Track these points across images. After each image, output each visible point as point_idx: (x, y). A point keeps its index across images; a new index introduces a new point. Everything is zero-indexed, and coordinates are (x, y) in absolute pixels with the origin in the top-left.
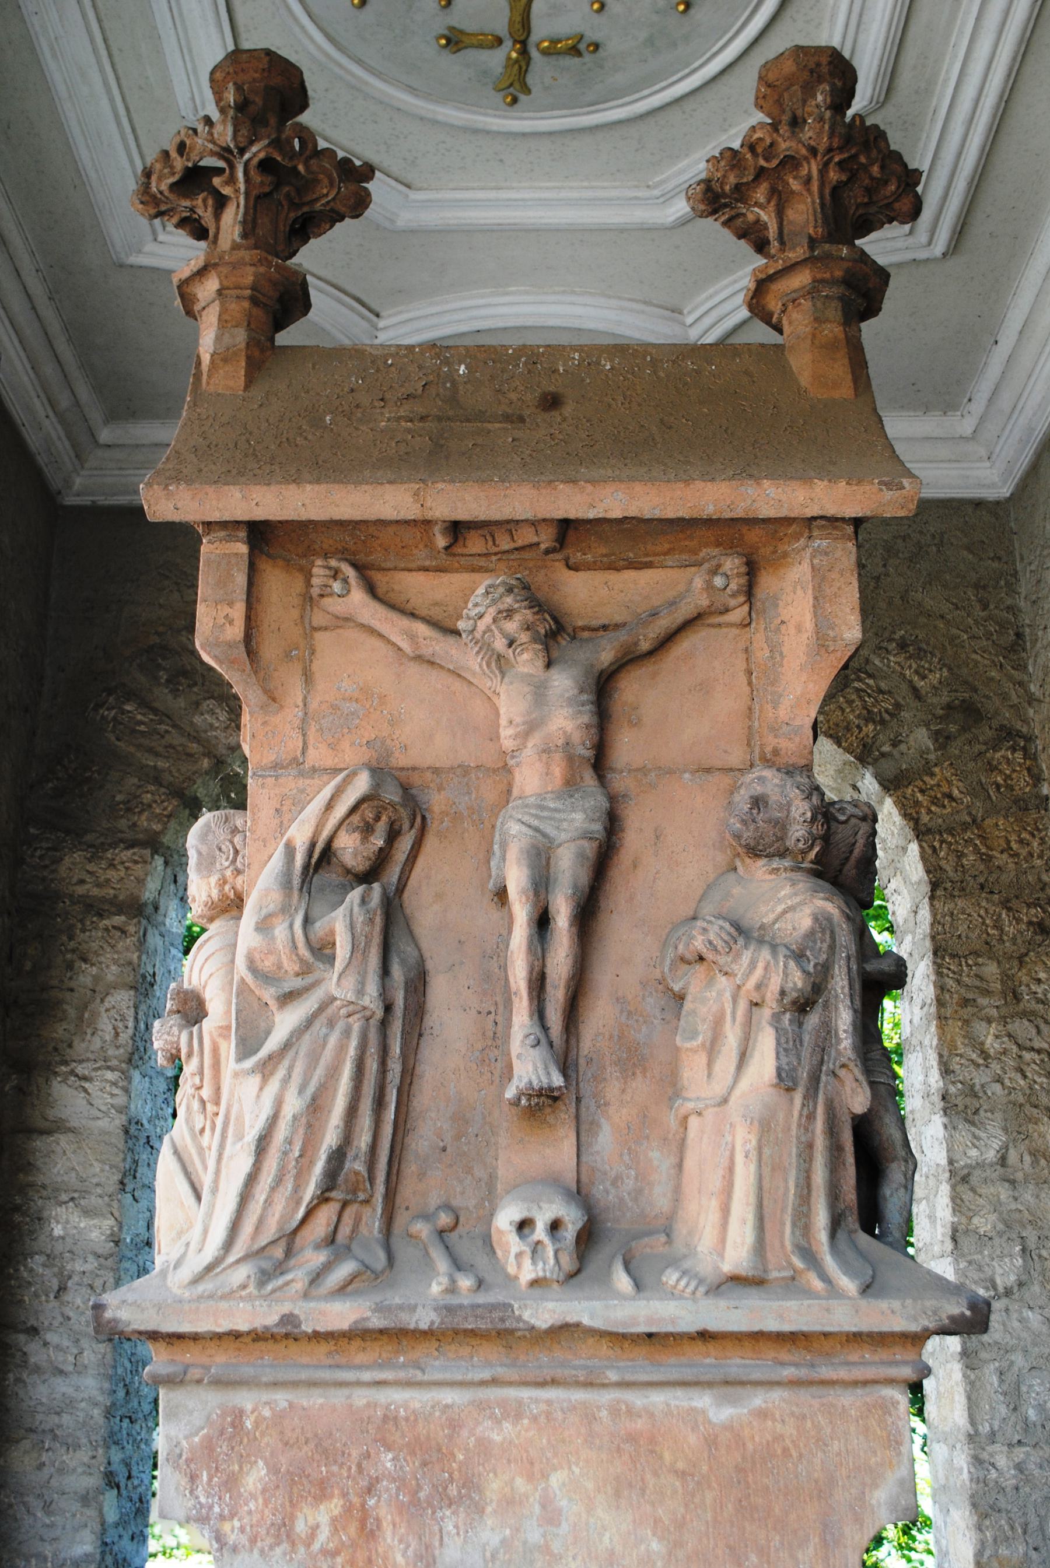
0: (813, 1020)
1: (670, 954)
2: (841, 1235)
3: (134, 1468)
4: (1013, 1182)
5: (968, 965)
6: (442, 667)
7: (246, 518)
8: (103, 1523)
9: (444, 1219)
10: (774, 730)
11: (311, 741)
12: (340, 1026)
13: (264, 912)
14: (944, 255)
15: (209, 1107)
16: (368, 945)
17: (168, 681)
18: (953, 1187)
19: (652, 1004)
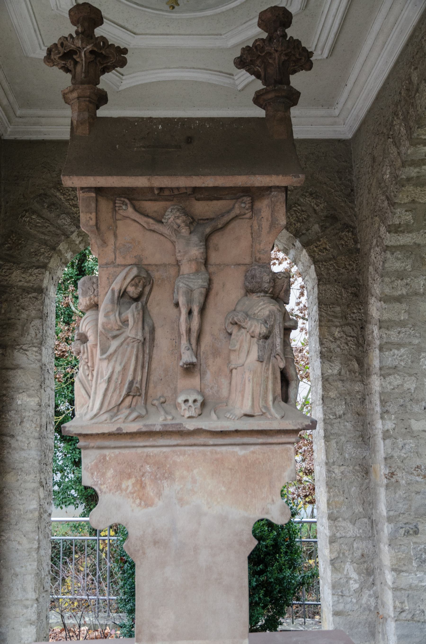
0: (269, 341)
1: (228, 322)
2: (276, 402)
3: (48, 480)
4: (343, 381)
5: (330, 308)
6: (157, 233)
7: (95, 186)
8: (40, 498)
9: (162, 400)
10: (259, 252)
11: (117, 256)
12: (131, 345)
13: (107, 311)
14: (327, 58)
15: (91, 368)
16: (138, 321)
17: (48, 207)
18: (323, 383)
19: (222, 336)
